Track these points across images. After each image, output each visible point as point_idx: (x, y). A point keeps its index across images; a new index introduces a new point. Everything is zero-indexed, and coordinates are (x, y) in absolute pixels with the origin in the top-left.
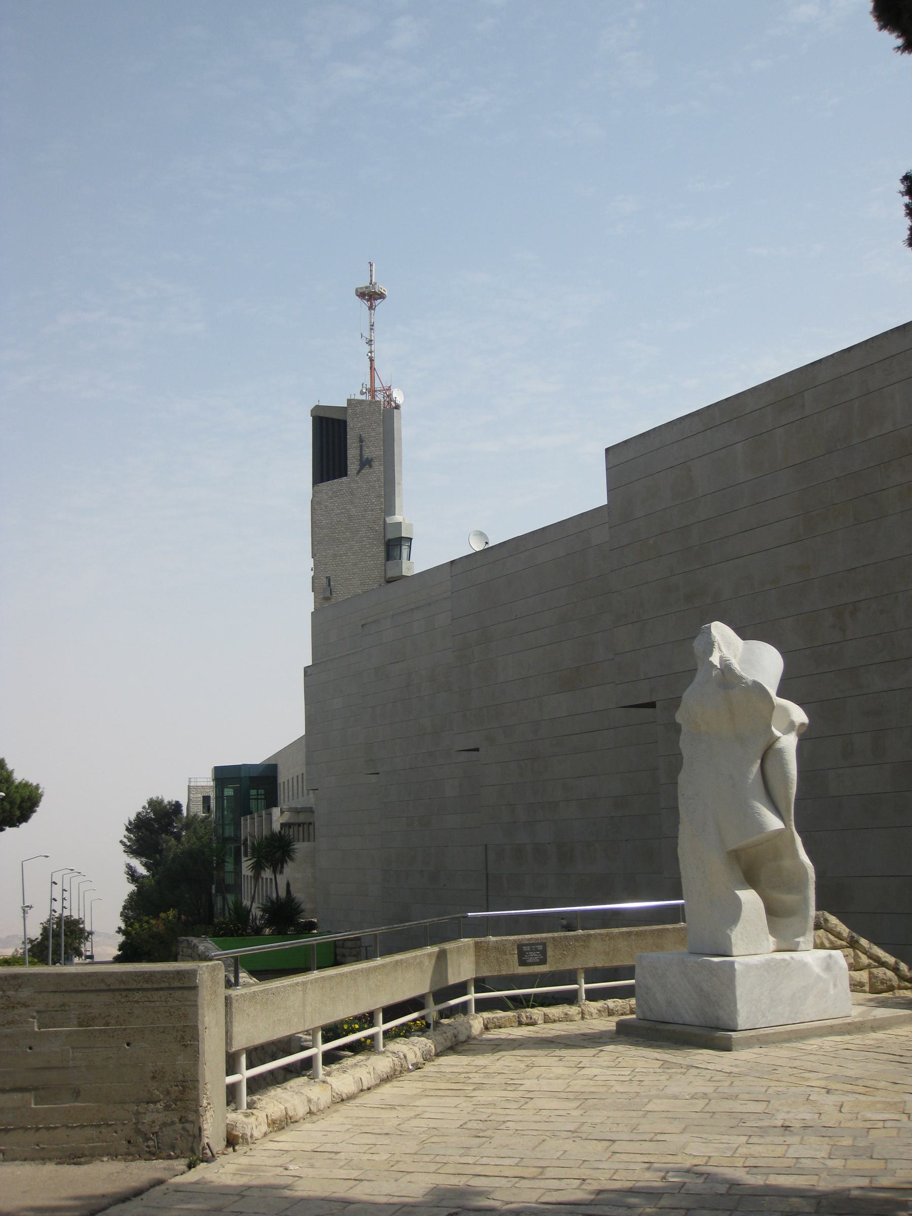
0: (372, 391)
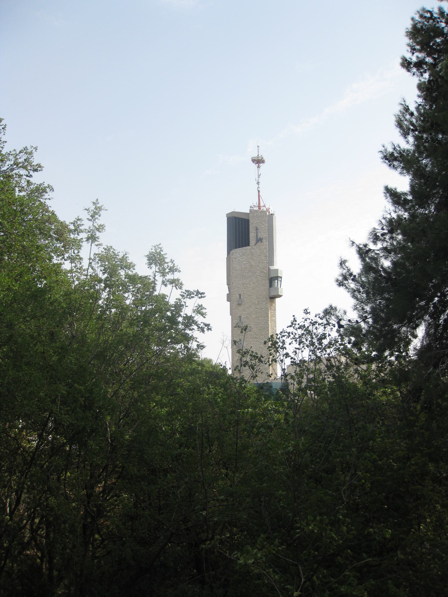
0: (259, 207)
